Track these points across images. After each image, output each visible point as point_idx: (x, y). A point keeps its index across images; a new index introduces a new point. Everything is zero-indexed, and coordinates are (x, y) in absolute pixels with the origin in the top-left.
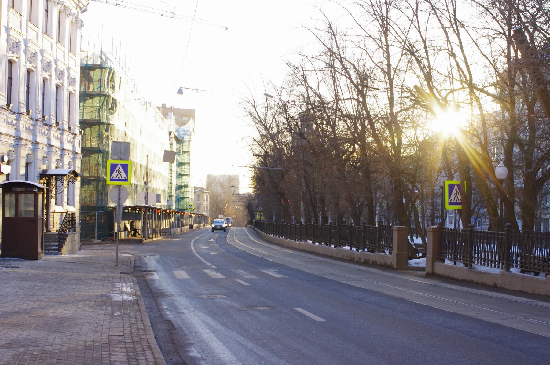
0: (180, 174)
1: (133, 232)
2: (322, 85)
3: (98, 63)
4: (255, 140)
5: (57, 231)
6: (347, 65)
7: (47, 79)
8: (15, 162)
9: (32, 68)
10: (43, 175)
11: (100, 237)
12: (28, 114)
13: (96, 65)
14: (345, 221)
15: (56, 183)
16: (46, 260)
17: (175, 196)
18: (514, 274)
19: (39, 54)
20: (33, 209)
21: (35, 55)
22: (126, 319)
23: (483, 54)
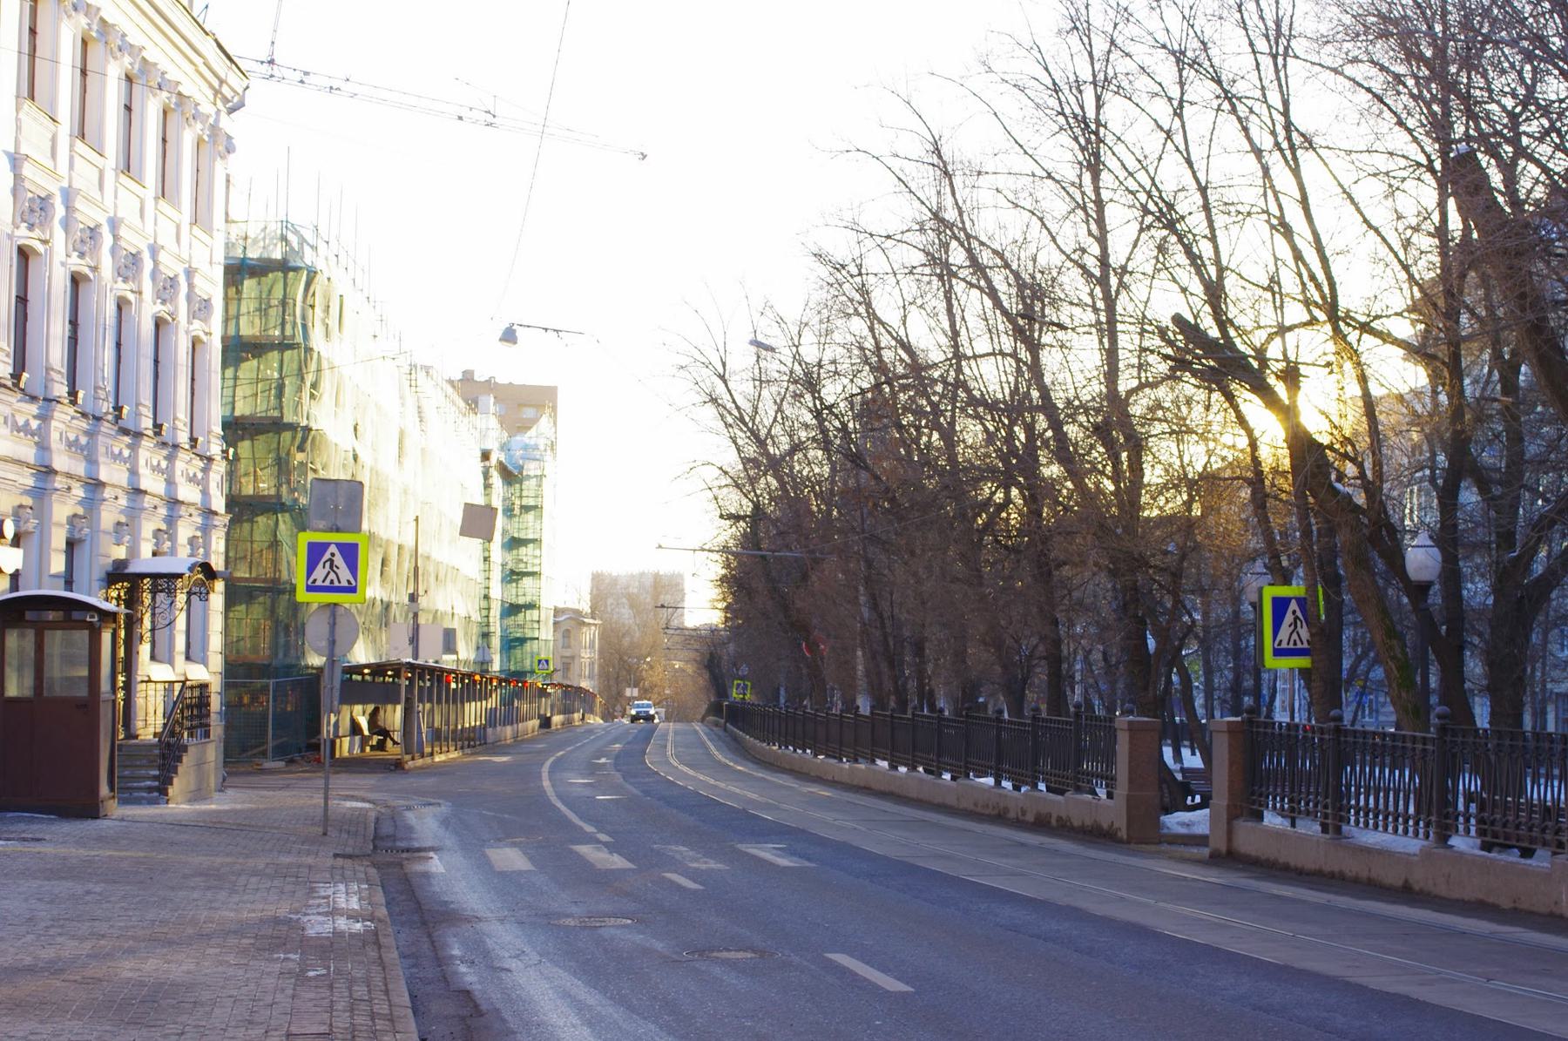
0: (513, 572)
1: (376, 739)
2: (914, 315)
3: (277, 255)
4: (726, 473)
5: (155, 735)
6: (986, 258)
7: (129, 303)
8: (35, 539)
9: (86, 271)
10: (117, 574)
11: (281, 752)
12: (74, 403)
13: (270, 260)
14: (985, 705)
15: (154, 599)
16: (122, 820)
17: (498, 633)
18: (1462, 854)
19: (105, 231)
20: (85, 672)
21: (93, 232)
22: (341, 985)
23: (1370, 226)
